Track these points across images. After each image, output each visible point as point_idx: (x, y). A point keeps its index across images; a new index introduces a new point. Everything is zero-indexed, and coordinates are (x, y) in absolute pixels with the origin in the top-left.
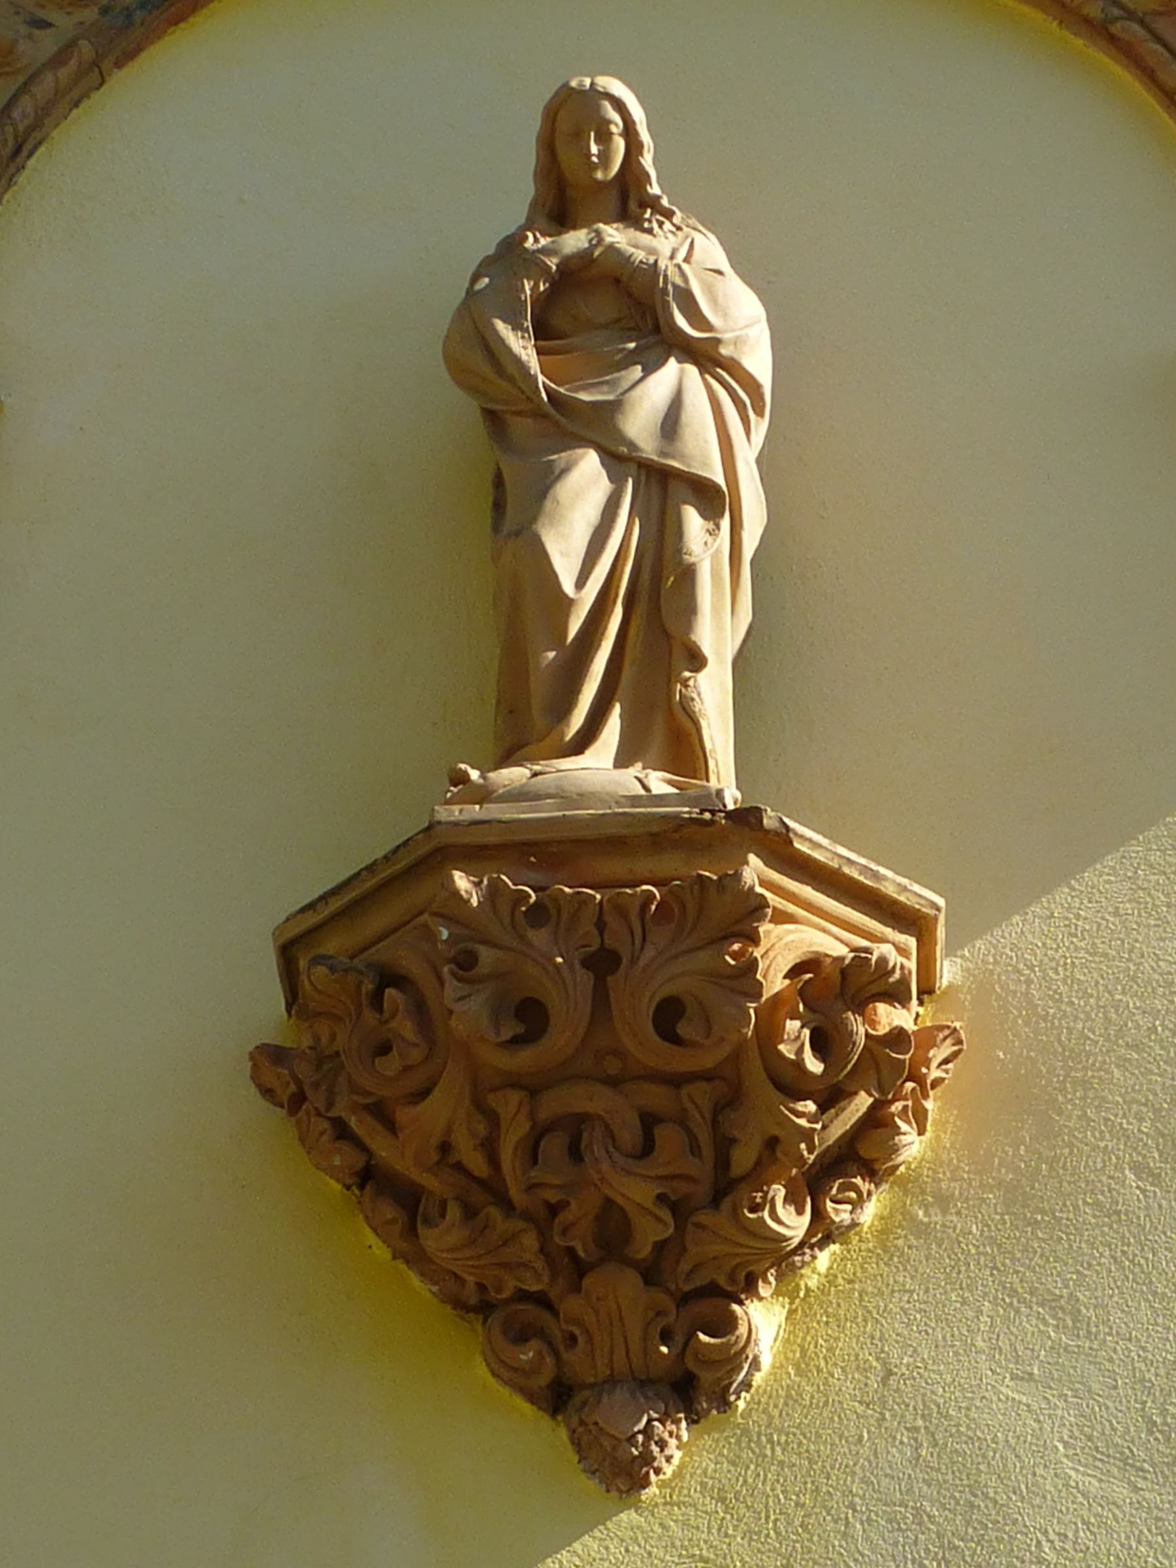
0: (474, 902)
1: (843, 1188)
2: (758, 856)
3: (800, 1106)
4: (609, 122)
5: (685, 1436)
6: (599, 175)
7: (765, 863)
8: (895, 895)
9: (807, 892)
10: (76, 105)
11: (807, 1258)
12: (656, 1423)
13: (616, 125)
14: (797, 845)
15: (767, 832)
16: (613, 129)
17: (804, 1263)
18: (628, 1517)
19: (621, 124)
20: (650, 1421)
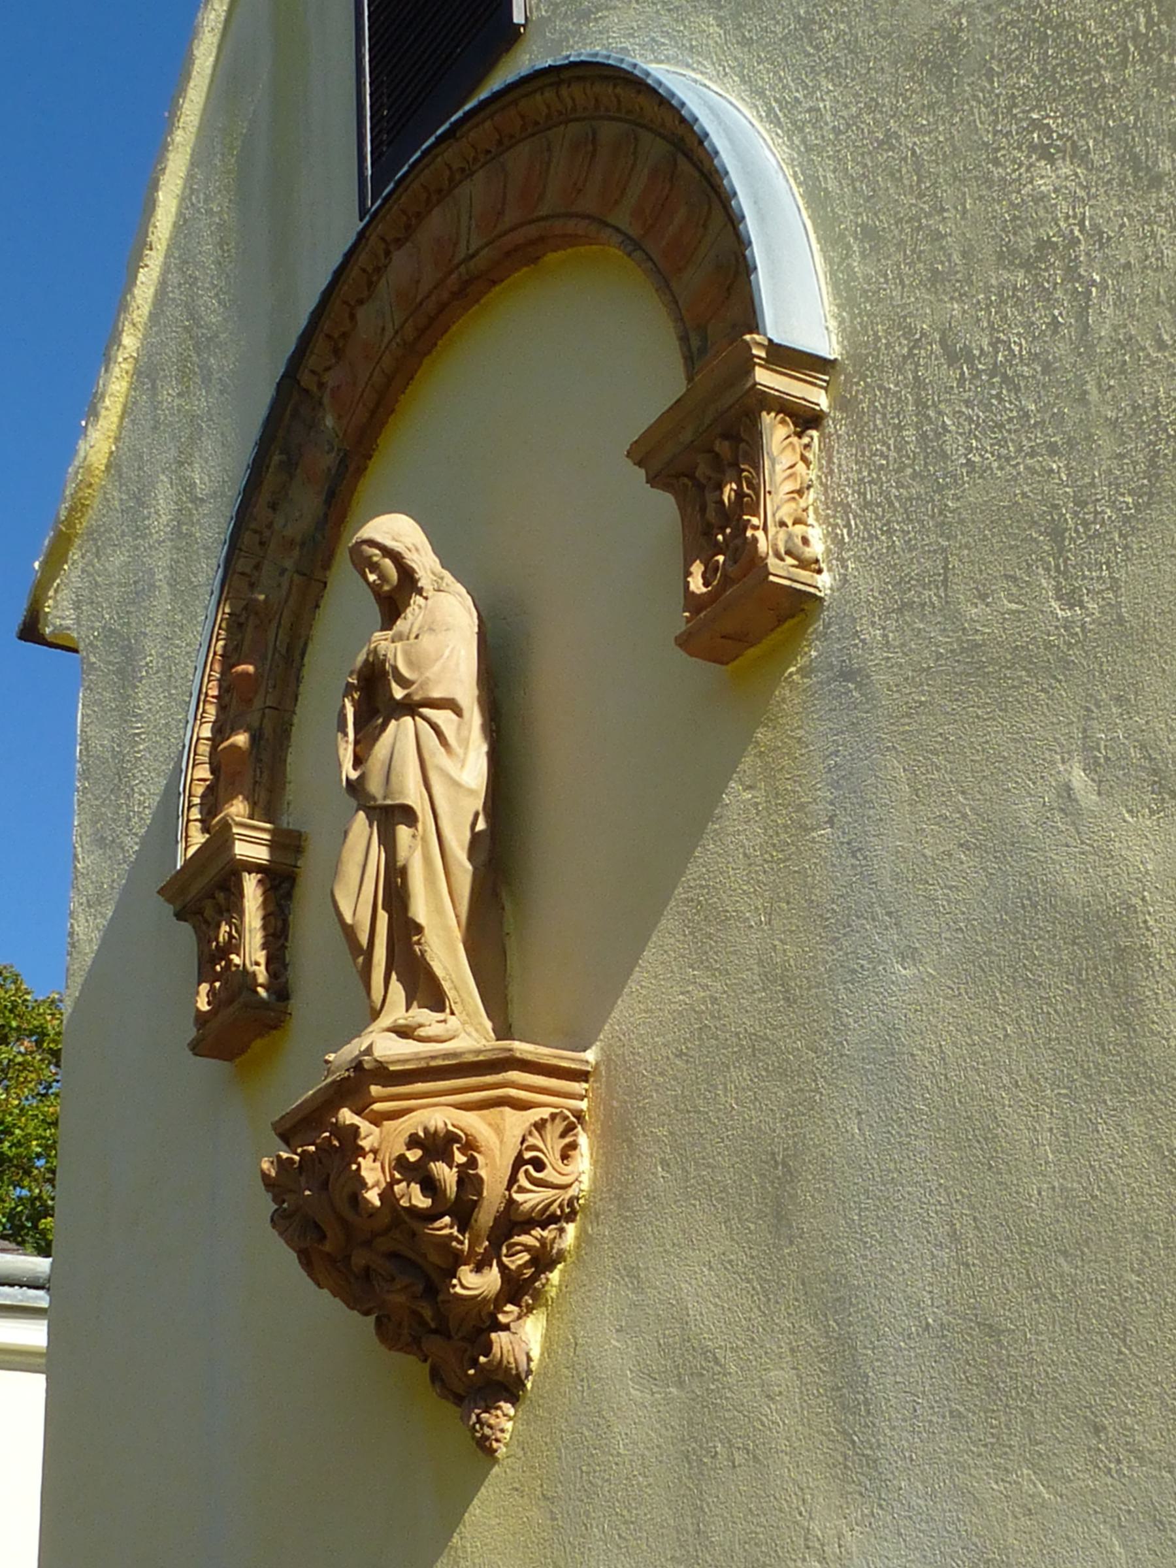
0: (273, 1174)
1: (509, 1247)
2: (376, 1084)
3: (437, 1224)
4: (370, 557)
5: (512, 1412)
6: (386, 588)
7: (384, 1086)
8: (476, 1059)
9: (420, 1087)
10: (317, 606)
11: (544, 1281)
12: (483, 1415)
13: (376, 555)
14: (392, 1068)
15: (369, 1070)
16: (375, 559)
17: (544, 1286)
18: (496, 1469)
19: (377, 552)
20: (478, 1416)
